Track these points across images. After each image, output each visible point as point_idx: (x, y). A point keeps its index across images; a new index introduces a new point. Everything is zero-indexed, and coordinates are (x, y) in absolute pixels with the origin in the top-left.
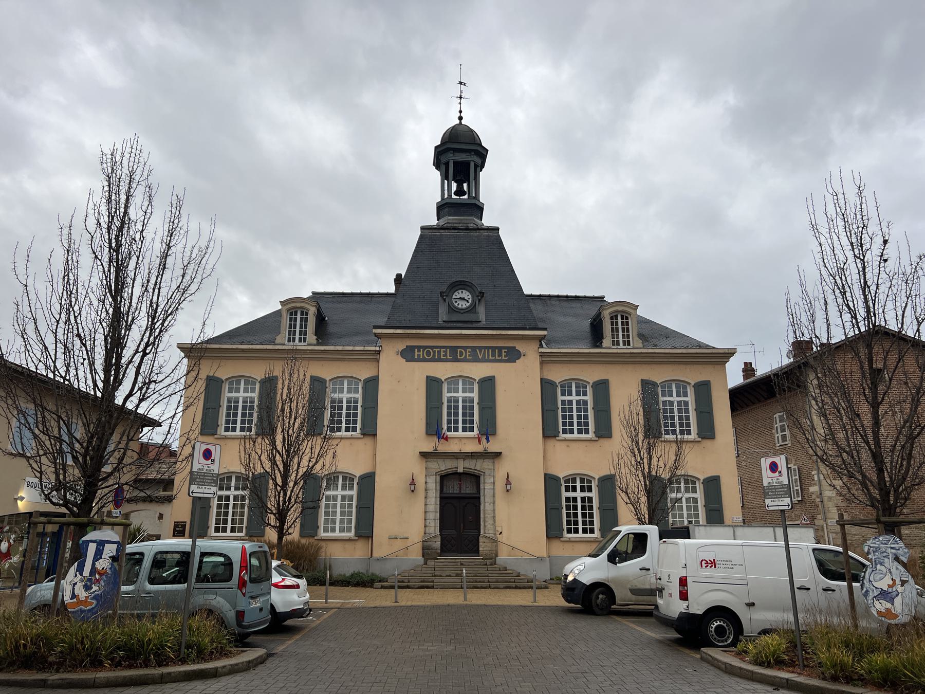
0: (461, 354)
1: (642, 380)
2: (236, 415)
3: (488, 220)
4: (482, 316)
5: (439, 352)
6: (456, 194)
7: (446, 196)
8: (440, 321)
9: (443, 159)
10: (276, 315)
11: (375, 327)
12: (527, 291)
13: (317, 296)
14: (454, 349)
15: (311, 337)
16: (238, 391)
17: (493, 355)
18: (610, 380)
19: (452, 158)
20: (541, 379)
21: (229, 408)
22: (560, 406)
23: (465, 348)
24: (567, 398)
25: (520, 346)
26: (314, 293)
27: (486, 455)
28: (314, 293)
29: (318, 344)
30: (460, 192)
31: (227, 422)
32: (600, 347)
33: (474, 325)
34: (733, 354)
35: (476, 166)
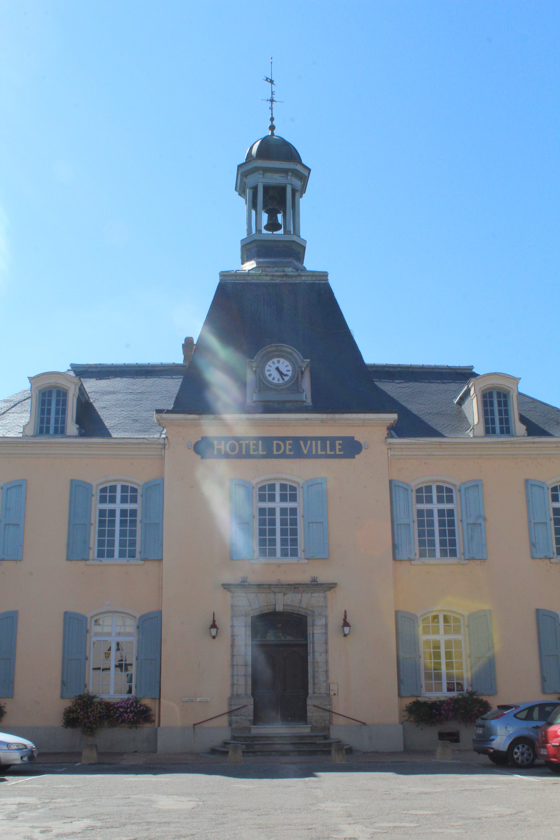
3: (312, 262)
6: (267, 228)
9: (251, 180)
18: (363, 452)
20: (391, 482)
26: (354, 458)
27: (315, 585)
28: (354, 458)
29: (81, 435)
30: (273, 226)
35: (294, 192)
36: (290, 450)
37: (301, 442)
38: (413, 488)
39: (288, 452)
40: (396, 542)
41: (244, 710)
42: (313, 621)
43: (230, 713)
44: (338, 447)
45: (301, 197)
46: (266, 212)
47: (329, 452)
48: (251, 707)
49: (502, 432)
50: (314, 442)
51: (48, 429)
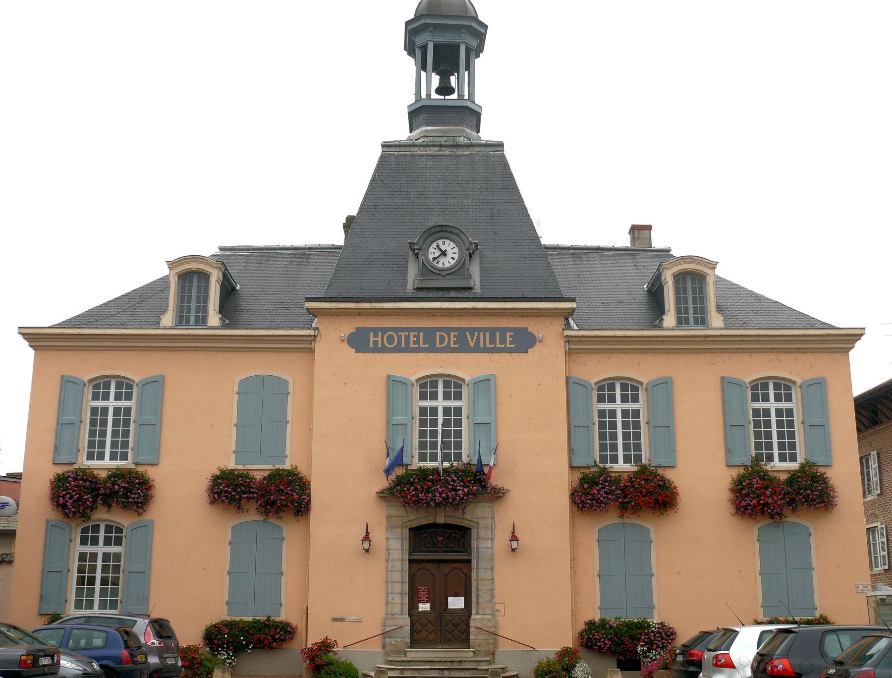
0: (442, 340)
1: (723, 378)
2: (115, 434)
3: (488, 133)
4: (476, 280)
5: (407, 338)
6: (438, 91)
7: (424, 96)
8: (410, 286)
9: (419, 40)
10: (158, 288)
11: (309, 299)
12: (546, 241)
13: (227, 255)
14: (430, 334)
15: (214, 319)
16: (106, 397)
17: (493, 341)
19: (429, 40)
20: (567, 379)
21: (93, 423)
22: (596, 419)
23: (448, 330)
24: (606, 406)
25: (534, 327)
29: (224, 326)
30: (445, 89)
31: (91, 444)
32: (660, 327)
33: (467, 294)
34: (858, 337)
36: (455, 343)
37: (468, 334)
38: (593, 385)
39: (452, 345)
40: (573, 447)
41: (399, 631)
42: (478, 534)
43: (384, 634)
44: (508, 339)
45: (478, 56)
46: (438, 74)
47: (498, 345)
48: (408, 629)
49: (696, 323)
50: (482, 334)
51: (188, 318)
